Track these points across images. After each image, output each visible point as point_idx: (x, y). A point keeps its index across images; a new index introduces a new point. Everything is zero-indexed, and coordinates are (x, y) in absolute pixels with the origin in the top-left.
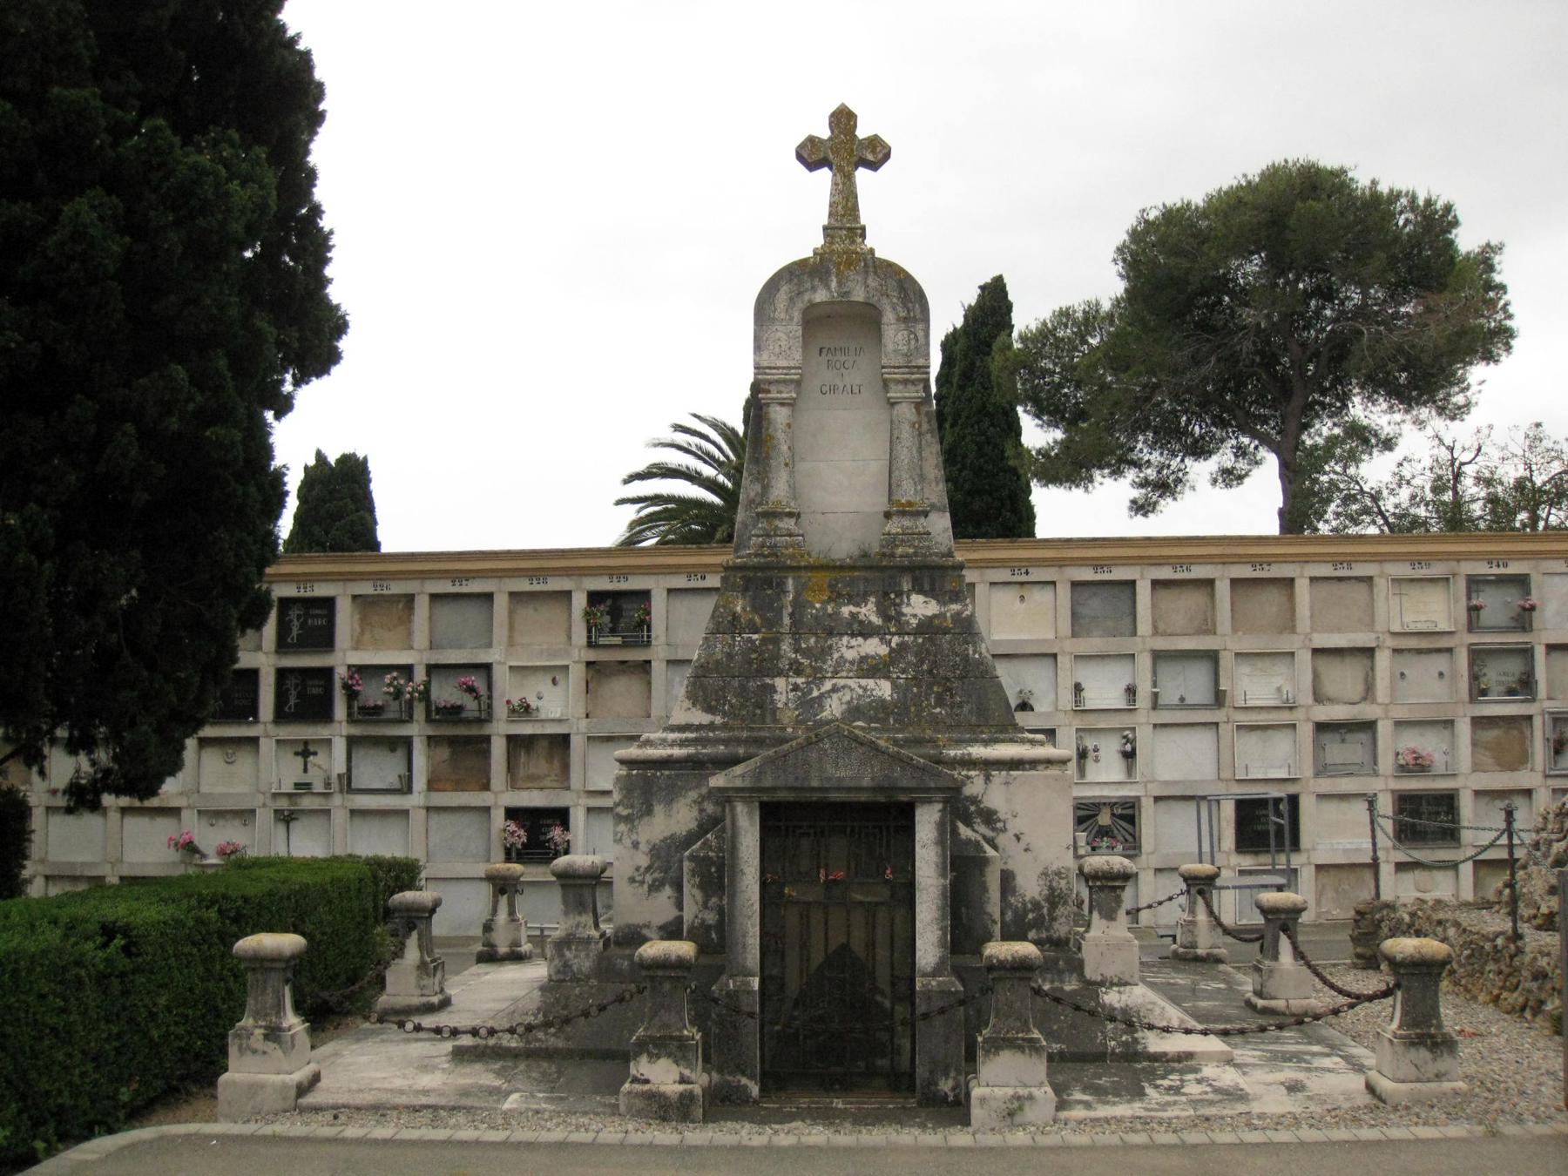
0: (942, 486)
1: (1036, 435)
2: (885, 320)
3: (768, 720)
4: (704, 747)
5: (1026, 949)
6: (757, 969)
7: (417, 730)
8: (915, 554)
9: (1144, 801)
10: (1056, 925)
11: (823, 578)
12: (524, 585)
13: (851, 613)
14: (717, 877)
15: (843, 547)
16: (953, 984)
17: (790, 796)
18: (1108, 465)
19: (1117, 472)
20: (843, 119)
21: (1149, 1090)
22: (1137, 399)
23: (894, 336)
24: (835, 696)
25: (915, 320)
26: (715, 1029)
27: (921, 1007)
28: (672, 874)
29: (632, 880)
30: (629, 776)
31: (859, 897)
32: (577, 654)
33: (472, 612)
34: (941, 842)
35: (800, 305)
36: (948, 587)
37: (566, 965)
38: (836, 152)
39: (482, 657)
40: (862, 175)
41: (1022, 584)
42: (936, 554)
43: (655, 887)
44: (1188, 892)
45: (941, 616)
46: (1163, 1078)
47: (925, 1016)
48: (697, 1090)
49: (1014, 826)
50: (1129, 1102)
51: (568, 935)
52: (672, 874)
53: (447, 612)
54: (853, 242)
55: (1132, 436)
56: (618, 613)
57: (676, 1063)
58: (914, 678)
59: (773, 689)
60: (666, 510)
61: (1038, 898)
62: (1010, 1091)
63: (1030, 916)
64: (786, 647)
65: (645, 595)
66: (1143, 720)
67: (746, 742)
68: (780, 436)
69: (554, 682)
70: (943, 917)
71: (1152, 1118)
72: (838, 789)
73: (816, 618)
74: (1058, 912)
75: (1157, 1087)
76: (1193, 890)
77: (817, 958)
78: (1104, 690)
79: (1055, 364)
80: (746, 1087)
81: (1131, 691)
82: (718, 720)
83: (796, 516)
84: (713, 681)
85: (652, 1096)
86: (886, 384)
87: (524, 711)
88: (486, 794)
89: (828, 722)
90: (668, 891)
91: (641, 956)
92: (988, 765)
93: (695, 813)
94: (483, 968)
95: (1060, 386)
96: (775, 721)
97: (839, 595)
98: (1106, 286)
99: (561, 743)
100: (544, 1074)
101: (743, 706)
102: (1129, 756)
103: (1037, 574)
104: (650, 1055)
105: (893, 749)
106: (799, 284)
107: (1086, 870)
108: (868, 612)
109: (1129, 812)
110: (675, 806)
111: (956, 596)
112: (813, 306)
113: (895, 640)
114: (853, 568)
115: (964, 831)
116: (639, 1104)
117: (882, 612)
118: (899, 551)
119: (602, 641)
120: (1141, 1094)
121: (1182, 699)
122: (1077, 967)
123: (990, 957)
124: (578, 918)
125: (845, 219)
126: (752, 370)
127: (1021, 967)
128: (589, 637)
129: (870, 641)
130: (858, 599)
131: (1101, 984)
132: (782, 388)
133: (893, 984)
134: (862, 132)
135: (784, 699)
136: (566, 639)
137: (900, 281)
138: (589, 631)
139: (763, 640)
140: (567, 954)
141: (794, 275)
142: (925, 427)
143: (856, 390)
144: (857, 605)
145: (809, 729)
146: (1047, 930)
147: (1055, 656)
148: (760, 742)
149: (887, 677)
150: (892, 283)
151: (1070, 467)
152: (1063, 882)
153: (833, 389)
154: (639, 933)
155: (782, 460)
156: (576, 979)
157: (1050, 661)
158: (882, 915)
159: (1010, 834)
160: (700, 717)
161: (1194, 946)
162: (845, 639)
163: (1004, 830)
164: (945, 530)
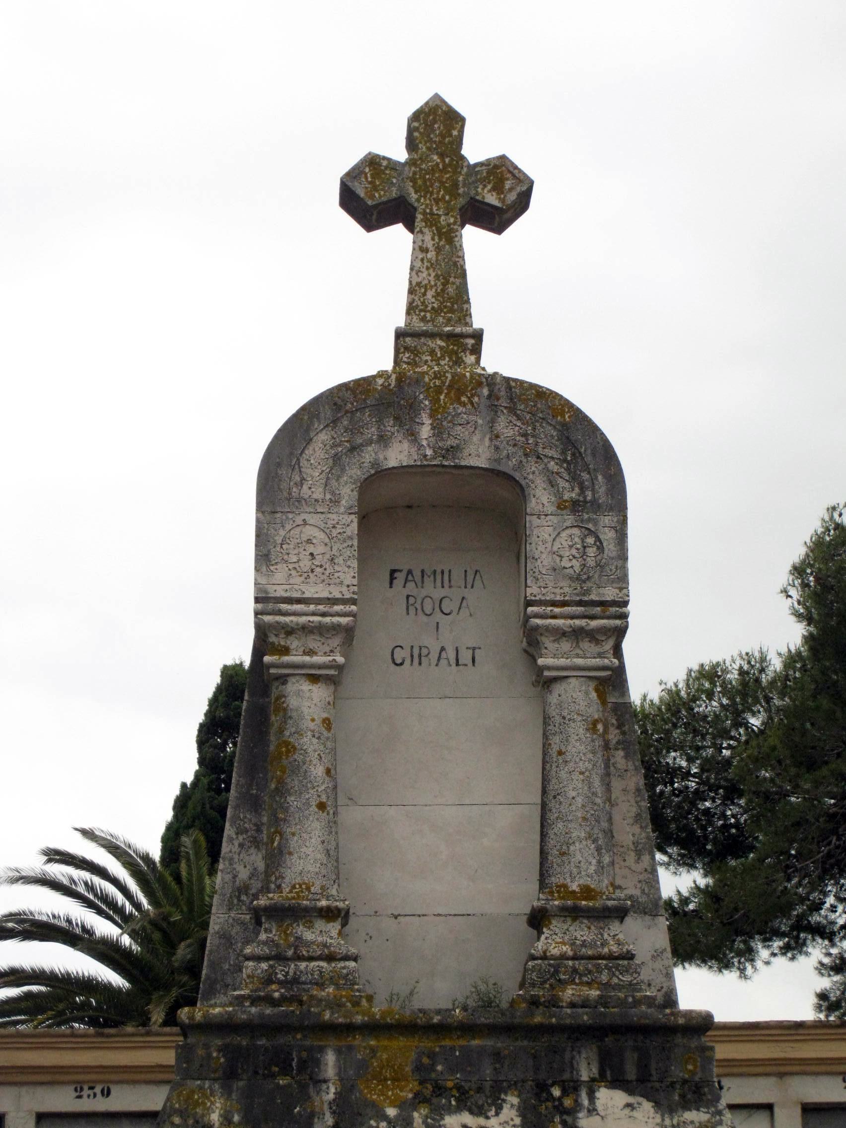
2: (532, 505)
8: (603, 1001)
11: (402, 1051)
15: (440, 991)
18: (780, 935)
19: (794, 948)
20: (436, 125)
22: (832, 817)
23: (551, 539)
25: (596, 506)
35: (355, 472)
36: (677, 1072)
38: (424, 190)
40: (474, 239)
54: (459, 362)
55: (818, 885)
60: (29, 995)
68: (310, 745)
79: (690, 760)
86: (532, 640)
95: (699, 795)
97: (439, 1090)
98: (777, 633)
114: (467, 1029)
118: (569, 993)
125: (440, 314)
126: (250, 606)
132: (313, 642)
134: (476, 149)
137: (564, 424)
141: (344, 408)
142: (614, 736)
143: (465, 657)
153: (419, 656)
155: (312, 797)
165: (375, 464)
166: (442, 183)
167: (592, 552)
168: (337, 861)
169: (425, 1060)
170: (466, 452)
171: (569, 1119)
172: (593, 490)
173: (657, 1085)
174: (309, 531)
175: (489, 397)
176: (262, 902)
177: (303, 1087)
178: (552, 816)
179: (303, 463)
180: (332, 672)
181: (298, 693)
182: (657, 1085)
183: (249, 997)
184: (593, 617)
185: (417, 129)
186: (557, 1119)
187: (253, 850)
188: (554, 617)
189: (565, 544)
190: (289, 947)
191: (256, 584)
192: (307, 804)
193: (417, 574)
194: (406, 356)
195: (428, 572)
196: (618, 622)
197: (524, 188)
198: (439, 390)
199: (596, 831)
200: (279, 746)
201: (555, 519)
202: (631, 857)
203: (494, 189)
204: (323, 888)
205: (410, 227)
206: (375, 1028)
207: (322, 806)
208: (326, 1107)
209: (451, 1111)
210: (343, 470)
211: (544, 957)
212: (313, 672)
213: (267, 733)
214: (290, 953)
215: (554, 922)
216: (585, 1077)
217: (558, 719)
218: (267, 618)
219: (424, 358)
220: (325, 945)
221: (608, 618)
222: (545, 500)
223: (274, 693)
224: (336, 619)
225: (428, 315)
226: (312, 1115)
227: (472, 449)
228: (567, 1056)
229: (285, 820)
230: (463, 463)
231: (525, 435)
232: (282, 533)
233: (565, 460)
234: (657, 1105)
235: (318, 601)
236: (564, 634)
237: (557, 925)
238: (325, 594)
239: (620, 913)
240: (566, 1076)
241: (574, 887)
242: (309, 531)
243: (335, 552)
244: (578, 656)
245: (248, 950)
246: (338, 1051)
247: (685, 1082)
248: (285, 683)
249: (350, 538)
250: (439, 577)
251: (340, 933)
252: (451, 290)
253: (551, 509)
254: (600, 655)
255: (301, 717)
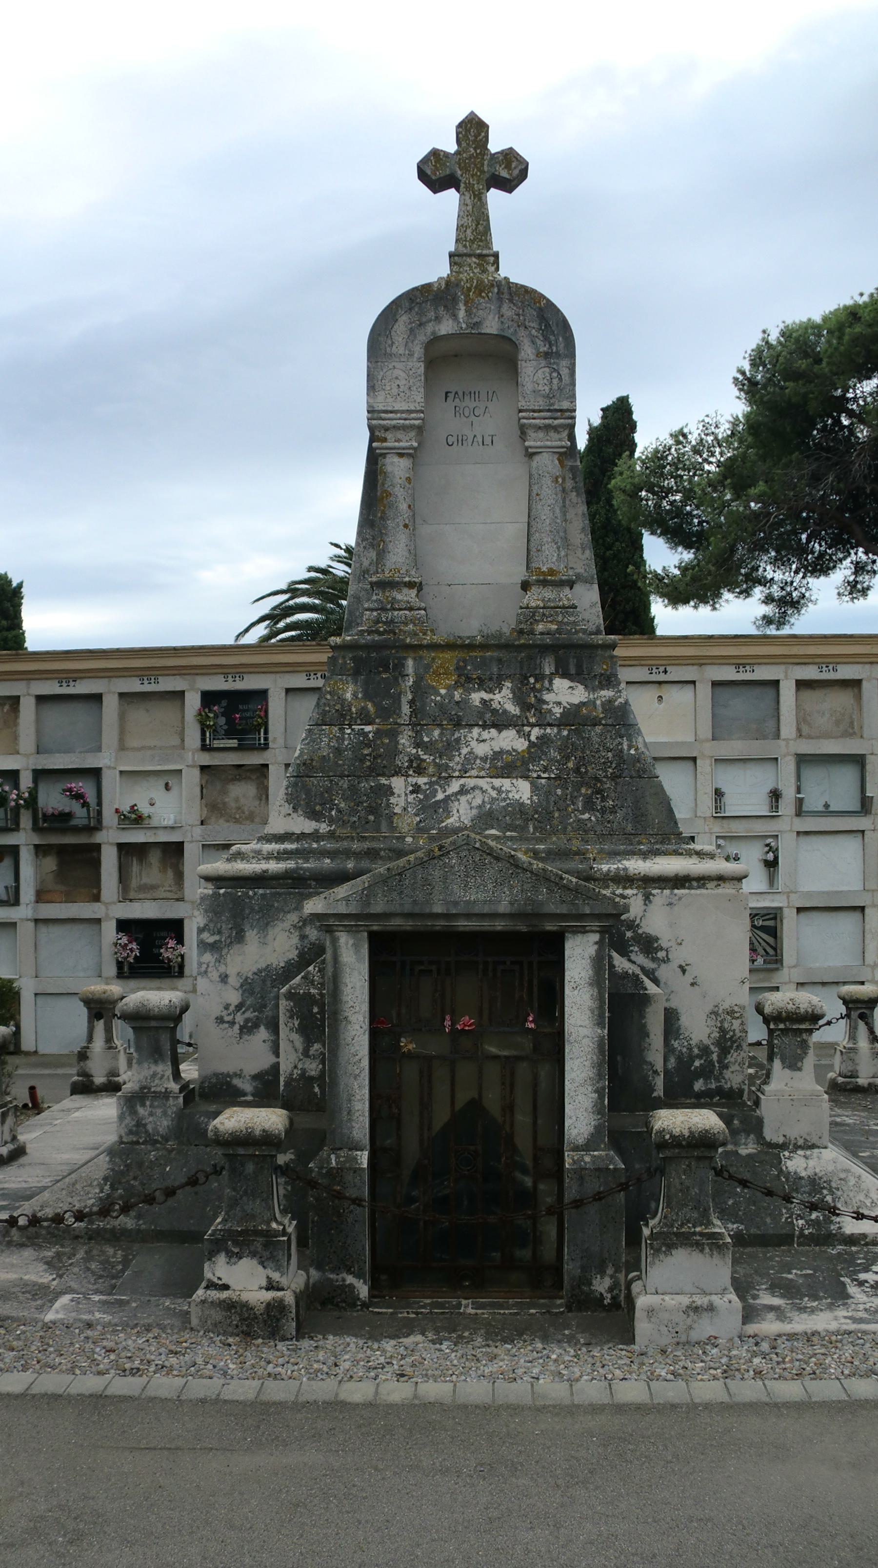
0: (589, 554)
1: (660, 556)
2: (522, 355)
3: (384, 827)
4: (307, 860)
5: (706, 1119)
6: (366, 1141)
7: (24, 838)
8: (559, 631)
9: (786, 912)
10: (727, 1074)
12: (134, 686)
13: (484, 702)
14: (318, 1020)
15: (471, 627)
16: (611, 1161)
17: (408, 925)
20: (473, 129)
21: (852, 1290)
23: (533, 373)
24: (463, 799)
25: (558, 355)
26: (313, 1216)
27: (571, 1192)
28: (268, 1012)
29: (220, 1020)
30: (216, 895)
31: (493, 1050)
32: (192, 757)
33: (80, 714)
34: (597, 981)
35: (422, 337)
36: (598, 669)
37: (140, 1124)
39: (91, 762)
40: (494, 197)
41: (660, 683)
42: (584, 631)
43: (248, 1028)
44: (848, 1016)
45: (590, 704)
46: (867, 1270)
47: (578, 1204)
48: (289, 1298)
49: (678, 956)
50: (831, 1307)
51: (143, 1088)
52: (268, 1012)
53: (55, 715)
54: (484, 271)
56: (235, 715)
57: (262, 1263)
58: (558, 778)
59: (389, 791)
61: (707, 1042)
62: (685, 1300)
63: (697, 1063)
64: (404, 740)
65: (262, 695)
66: (787, 827)
67: (358, 855)
69: (167, 787)
70: (600, 1076)
71: (865, 1332)
72: (468, 916)
73: (441, 706)
74: (730, 1059)
75: (861, 1283)
76: (855, 1014)
77: (441, 1116)
78: (747, 793)
80: (352, 1287)
81: (775, 795)
82: (324, 828)
83: (418, 586)
84: (317, 782)
85: (230, 1306)
86: (523, 431)
87: (134, 818)
88: (97, 905)
89: (455, 831)
90: (263, 1033)
91: (216, 1131)
92: (648, 882)
93: (295, 940)
94: (79, 1100)
96: (392, 828)
97: (469, 679)
98: (730, 407)
99: (174, 852)
100: (105, 1263)
101: (353, 812)
102: (771, 865)
103: (676, 673)
104: (230, 1255)
105: (537, 865)
106: (421, 314)
107: (767, 1010)
108: (503, 699)
109: (771, 923)
110: (272, 932)
111: (609, 680)
112: (436, 339)
113: (535, 732)
114: (484, 647)
115: (621, 963)
116: (217, 1315)
117: (519, 699)
118: (540, 627)
119: (217, 744)
120: (841, 1296)
121: (827, 806)
122: (756, 1126)
123: (661, 1132)
124: (153, 1068)
125: (474, 241)
127: (701, 1144)
128: (203, 740)
129: (505, 733)
130: (490, 683)
131: (783, 1146)
132: (400, 435)
133: (536, 1159)
134: (495, 145)
135: (402, 804)
136: (183, 740)
137: (541, 309)
138: (203, 733)
139: (377, 733)
140: (141, 1111)
141: (417, 302)
142: (569, 484)
143: (488, 440)
144: (491, 691)
145: (432, 839)
146: (717, 1080)
147: (694, 759)
148: (372, 854)
149: (526, 777)
150: (531, 313)
151: (690, 589)
152: (736, 1024)
153: (461, 440)
154: (229, 1084)
155: (400, 521)
156: (151, 1141)
157: (690, 764)
158: (523, 1069)
159: (674, 965)
160: (303, 825)
161: (854, 1075)
162: (476, 731)
163: (666, 960)
164: (593, 605)
165: (433, 333)
166: (475, 165)
167: (555, 381)
168: (415, 556)
169: (461, 664)
170: (484, 325)
171: (538, 695)
172: (557, 346)
173: (587, 676)
174: (397, 372)
175: (498, 293)
176: (374, 579)
177: (396, 679)
178: (533, 530)
179: (393, 333)
180: (411, 451)
181: (392, 463)
182: (587, 676)
183: (367, 630)
184: (555, 419)
185: (461, 133)
186: (532, 695)
187: (371, 550)
188: (534, 419)
189: (541, 377)
190: (388, 603)
191: (368, 403)
192: (398, 525)
193: (460, 394)
194: (455, 268)
195: (467, 393)
196: (570, 421)
197: (523, 167)
198: (469, 290)
199: (557, 537)
200: (382, 493)
201: (534, 363)
202: (579, 552)
203: (505, 167)
204: (407, 571)
205: (458, 190)
206: (434, 647)
207: (406, 526)
208: (408, 689)
209: (475, 691)
210: (415, 337)
211: (527, 608)
212: (400, 451)
213: (377, 485)
214: (389, 606)
215: (533, 588)
216: (547, 673)
217: (536, 476)
218: (374, 422)
219: (465, 268)
220: (408, 602)
221: (565, 418)
222: (529, 352)
223: (380, 463)
224: (412, 422)
225: (468, 244)
226: (400, 694)
227: (487, 323)
228: (538, 662)
229: (386, 534)
230: (483, 332)
231: (518, 315)
232: (382, 373)
233: (541, 329)
234: (586, 687)
235: (402, 412)
236: (540, 428)
237: (534, 589)
238: (405, 408)
239: (571, 584)
240: (537, 672)
241: (544, 569)
242: (397, 372)
243: (411, 383)
244: (547, 440)
245: (366, 606)
246: (415, 659)
247: (602, 675)
248: (384, 458)
249: (420, 376)
250: (473, 395)
251: (417, 595)
252: (481, 228)
253: (532, 357)
254: (560, 440)
255: (394, 477)
